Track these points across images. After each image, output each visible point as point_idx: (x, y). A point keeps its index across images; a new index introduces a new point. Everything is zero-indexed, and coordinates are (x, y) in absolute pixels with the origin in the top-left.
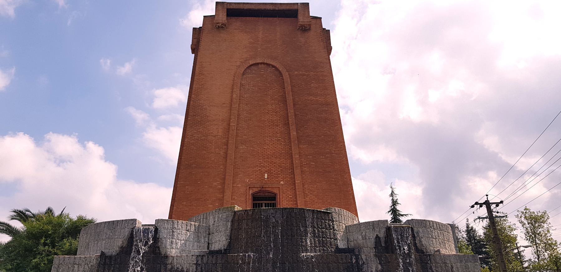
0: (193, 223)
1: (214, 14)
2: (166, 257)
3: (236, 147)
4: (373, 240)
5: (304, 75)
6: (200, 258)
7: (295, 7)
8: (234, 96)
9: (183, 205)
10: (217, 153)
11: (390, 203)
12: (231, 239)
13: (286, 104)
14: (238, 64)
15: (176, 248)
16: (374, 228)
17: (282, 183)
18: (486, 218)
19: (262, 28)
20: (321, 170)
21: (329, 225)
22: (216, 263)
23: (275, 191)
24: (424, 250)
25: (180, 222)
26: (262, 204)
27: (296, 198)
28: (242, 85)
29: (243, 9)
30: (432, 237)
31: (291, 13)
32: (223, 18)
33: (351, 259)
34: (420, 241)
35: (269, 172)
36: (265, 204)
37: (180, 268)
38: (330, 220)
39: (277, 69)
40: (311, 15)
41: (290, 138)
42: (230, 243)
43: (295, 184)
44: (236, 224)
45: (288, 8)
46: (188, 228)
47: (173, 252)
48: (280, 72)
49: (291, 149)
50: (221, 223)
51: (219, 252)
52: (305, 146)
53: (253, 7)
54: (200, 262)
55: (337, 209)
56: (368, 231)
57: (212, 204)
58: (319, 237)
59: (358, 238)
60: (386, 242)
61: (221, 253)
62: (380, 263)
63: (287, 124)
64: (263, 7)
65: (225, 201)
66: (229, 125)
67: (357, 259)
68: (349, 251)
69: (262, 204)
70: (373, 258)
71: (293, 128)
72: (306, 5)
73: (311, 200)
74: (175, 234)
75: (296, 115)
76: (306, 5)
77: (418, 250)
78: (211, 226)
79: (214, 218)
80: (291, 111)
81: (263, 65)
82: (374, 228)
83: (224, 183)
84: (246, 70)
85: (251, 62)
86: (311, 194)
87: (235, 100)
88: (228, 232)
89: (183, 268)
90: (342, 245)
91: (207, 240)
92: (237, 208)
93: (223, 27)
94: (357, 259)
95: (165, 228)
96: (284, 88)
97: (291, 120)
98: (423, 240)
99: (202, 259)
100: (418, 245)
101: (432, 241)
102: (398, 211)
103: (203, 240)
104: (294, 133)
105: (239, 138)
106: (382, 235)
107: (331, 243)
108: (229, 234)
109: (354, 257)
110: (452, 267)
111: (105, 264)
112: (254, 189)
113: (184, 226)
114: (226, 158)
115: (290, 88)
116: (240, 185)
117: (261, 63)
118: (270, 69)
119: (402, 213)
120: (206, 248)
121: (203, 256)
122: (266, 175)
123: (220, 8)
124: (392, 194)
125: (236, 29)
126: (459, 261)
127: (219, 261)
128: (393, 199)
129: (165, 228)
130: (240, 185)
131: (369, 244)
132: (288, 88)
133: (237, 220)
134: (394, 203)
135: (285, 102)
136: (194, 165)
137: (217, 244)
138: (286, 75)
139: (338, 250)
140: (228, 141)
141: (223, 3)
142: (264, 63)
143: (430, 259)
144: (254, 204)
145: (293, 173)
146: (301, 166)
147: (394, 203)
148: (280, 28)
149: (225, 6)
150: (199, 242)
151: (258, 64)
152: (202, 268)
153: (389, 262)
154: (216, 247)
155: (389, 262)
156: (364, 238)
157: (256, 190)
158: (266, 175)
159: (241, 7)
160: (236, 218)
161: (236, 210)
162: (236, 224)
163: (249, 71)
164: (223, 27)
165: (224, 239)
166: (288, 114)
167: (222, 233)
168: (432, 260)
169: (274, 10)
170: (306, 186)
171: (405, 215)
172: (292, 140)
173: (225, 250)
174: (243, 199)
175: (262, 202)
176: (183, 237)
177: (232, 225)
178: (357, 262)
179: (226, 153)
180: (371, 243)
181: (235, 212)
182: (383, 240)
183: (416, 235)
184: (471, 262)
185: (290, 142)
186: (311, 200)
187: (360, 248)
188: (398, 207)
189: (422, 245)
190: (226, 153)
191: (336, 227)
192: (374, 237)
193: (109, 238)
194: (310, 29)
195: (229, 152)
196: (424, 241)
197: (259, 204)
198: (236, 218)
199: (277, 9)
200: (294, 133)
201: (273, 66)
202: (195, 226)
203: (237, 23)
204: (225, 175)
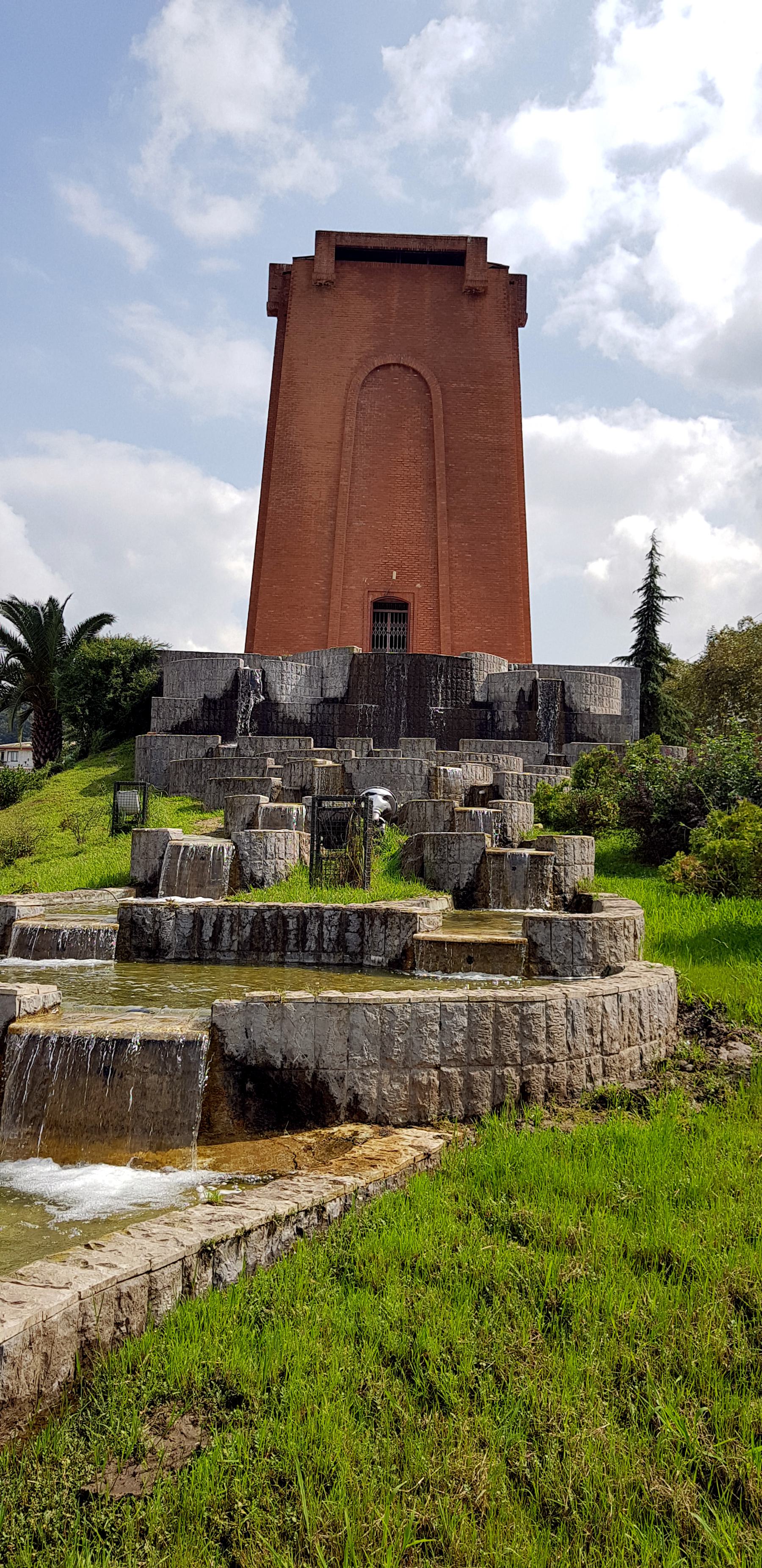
0: (304, 665)
1: (312, 253)
2: (278, 704)
3: (350, 524)
4: (516, 694)
5: (466, 390)
6: (315, 707)
7: (461, 247)
8: (347, 429)
11: (645, 572)
12: (349, 686)
13: (433, 446)
14: (354, 363)
17: (418, 585)
19: (397, 277)
20: (480, 567)
21: (467, 674)
22: (333, 714)
23: (408, 598)
26: (386, 614)
27: (438, 611)
28: (360, 407)
30: (586, 693)
31: (453, 259)
32: (327, 267)
33: (486, 715)
34: (571, 697)
35: (398, 567)
36: (392, 614)
39: (421, 377)
40: (489, 260)
41: (435, 511)
42: (348, 691)
43: (438, 588)
44: (355, 669)
45: (448, 247)
47: (283, 699)
48: (426, 383)
49: (435, 530)
50: (337, 666)
51: (334, 700)
52: (459, 525)
54: (315, 712)
55: (478, 653)
58: (452, 688)
59: (499, 689)
60: (530, 697)
61: (337, 702)
62: (518, 721)
65: (331, 612)
66: (338, 482)
67: (493, 715)
68: (487, 705)
69: (386, 614)
70: (511, 715)
71: (441, 492)
72: (482, 242)
75: (448, 468)
76: (482, 242)
77: (565, 707)
78: (325, 669)
79: (328, 659)
80: (441, 461)
81: (397, 368)
83: (330, 583)
84: (367, 377)
87: (348, 438)
88: (346, 678)
90: (479, 698)
92: (357, 650)
94: (493, 715)
95: (272, 671)
96: (432, 417)
100: (567, 702)
102: (659, 588)
105: (353, 507)
106: (527, 689)
107: (466, 695)
109: (489, 713)
110: (600, 728)
111: (209, 708)
112: (376, 594)
113: (294, 670)
114: (333, 540)
115: (441, 416)
116: (353, 587)
117: (394, 364)
118: (409, 377)
119: (665, 594)
120: (319, 694)
122: (395, 573)
123: (323, 244)
124: (651, 553)
125: (351, 289)
127: (336, 711)
128: (651, 565)
129: (272, 671)
130: (353, 587)
131: (511, 698)
133: (356, 663)
134: (654, 572)
135: (431, 442)
136: (283, 552)
137: (332, 691)
139: (475, 704)
140: (336, 512)
141: (329, 233)
142: (399, 365)
144: (374, 613)
145: (436, 570)
146: (450, 560)
147: (654, 572)
148: (432, 284)
149: (333, 242)
151: (389, 365)
153: (529, 720)
154: (331, 694)
155: (529, 720)
156: (507, 690)
157: (378, 596)
158: (395, 573)
160: (356, 662)
161: (355, 651)
162: (355, 669)
165: (341, 685)
166: (434, 466)
167: (339, 679)
168: (579, 720)
169: (421, 251)
170: (455, 592)
171: (670, 598)
172: (439, 515)
175: (387, 611)
177: (351, 670)
178: (492, 719)
179: (333, 533)
180: (513, 697)
181: (354, 655)
182: (527, 695)
185: (436, 517)
187: (499, 702)
188: (658, 581)
190: (333, 533)
191: (474, 676)
193: (209, 679)
194: (485, 293)
195: (338, 532)
196: (575, 698)
197: (382, 613)
198: (356, 662)
199: (428, 249)
200: (442, 502)
201: (415, 371)
203: (353, 273)
204: (331, 570)
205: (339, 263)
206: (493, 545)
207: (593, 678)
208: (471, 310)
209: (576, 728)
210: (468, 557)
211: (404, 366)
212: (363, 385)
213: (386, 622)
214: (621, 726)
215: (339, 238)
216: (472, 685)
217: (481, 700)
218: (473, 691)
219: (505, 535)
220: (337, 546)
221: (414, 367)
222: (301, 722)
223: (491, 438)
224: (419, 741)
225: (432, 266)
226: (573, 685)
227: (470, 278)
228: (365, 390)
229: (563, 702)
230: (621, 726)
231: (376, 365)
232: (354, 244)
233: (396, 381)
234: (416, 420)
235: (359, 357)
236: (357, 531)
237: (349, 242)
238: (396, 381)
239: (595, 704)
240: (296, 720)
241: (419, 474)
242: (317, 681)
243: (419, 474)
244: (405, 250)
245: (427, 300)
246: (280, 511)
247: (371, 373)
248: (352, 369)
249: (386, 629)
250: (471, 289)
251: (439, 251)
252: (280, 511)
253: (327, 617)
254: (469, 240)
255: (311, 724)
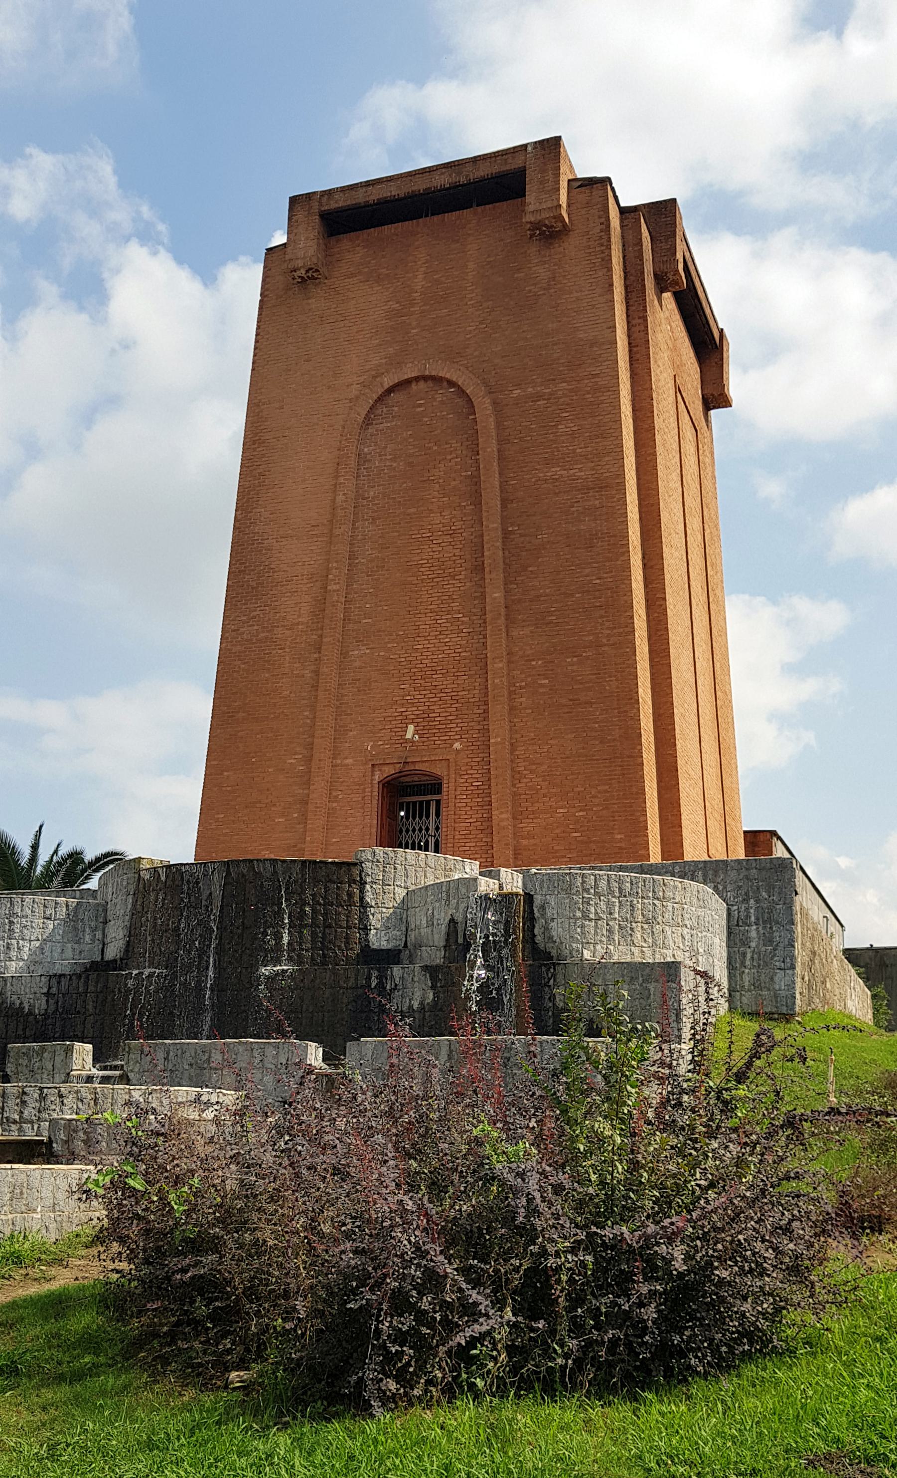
0: (62, 900)
3: (344, 654)
4: (444, 928)
6: (54, 981)
8: (340, 498)
9: (217, 820)
10: (297, 676)
14: (355, 390)
15: (17, 959)
16: (448, 899)
17: (457, 745)
18: (102, 958)
19: (422, 241)
20: (564, 701)
21: (350, 895)
23: (439, 770)
24: (554, 953)
25: (28, 899)
26: (428, 802)
28: (362, 459)
29: (367, 205)
30: (586, 917)
31: (505, 192)
33: (369, 978)
34: (546, 929)
37: (18, 1002)
38: (355, 882)
39: (461, 392)
46: (48, 913)
52: (527, 631)
53: (392, 191)
54: (54, 990)
56: (437, 904)
57: (282, 816)
62: (433, 987)
63: (479, 568)
64: (420, 185)
69: (428, 802)
71: (495, 577)
72: (551, 148)
73: (530, 789)
74: (17, 928)
75: (506, 535)
76: (551, 148)
81: (422, 384)
82: (448, 899)
85: (388, 381)
86: (532, 772)
89: (21, 1003)
91: (99, 935)
93: (313, 278)
97: (494, 551)
98: (553, 925)
99: (59, 983)
100: (539, 939)
101: (583, 926)
103: (88, 938)
104: (495, 595)
108: (128, 924)
109: (375, 974)
112: (386, 768)
115: (493, 447)
116: (349, 761)
117: (417, 379)
118: (442, 394)
121: (61, 975)
123: (300, 216)
125: (352, 275)
126: (627, 979)
127: (91, 988)
130: (349, 761)
132: (489, 446)
136: (241, 715)
138: (484, 406)
142: (425, 378)
143: (554, 975)
146: (510, 693)
148: (477, 235)
150: (78, 942)
151: (408, 382)
152: (57, 1003)
156: (431, 924)
157: (389, 771)
159: (360, 197)
163: (382, 410)
164: (313, 278)
167: (120, 921)
168: (560, 977)
169: (455, 187)
173: (121, 959)
174: (357, 798)
176: (37, 933)
183: (537, 914)
184: (657, 981)
186: (530, 789)
189: (551, 938)
192: (447, 920)
196: (556, 930)
197: (421, 803)
199: (463, 180)
200: (495, 595)
201: (451, 384)
202: (67, 906)
203: (354, 250)
205: (333, 240)
206: (588, 658)
207: (603, 884)
208: (545, 262)
209: (552, 998)
210: (543, 686)
211: (433, 378)
212: (368, 421)
213: (428, 817)
214: (652, 987)
215: (325, 199)
216: (364, 916)
217: (384, 945)
218: (366, 929)
219: (608, 636)
220: (321, 695)
221: (448, 376)
222: (30, 1013)
223: (580, 470)
224: (43, 1049)
225: (480, 209)
226: (552, 900)
227: (531, 208)
228: (371, 430)
229: (530, 938)
230: (652, 987)
231: (386, 386)
232: (349, 203)
233: (420, 405)
234: (453, 463)
235: (362, 379)
236: (357, 664)
237: (340, 202)
238: (420, 405)
239: (610, 939)
240: (21, 1008)
241: (457, 552)
242: (94, 930)
243: (457, 552)
244: (428, 192)
245: (471, 265)
246: (239, 648)
247: (380, 399)
248: (351, 400)
249: (427, 829)
250: (536, 226)
251: (482, 180)
252: (239, 648)
253: (304, 818)
254: (529, 148)
255: (46, 1015)
